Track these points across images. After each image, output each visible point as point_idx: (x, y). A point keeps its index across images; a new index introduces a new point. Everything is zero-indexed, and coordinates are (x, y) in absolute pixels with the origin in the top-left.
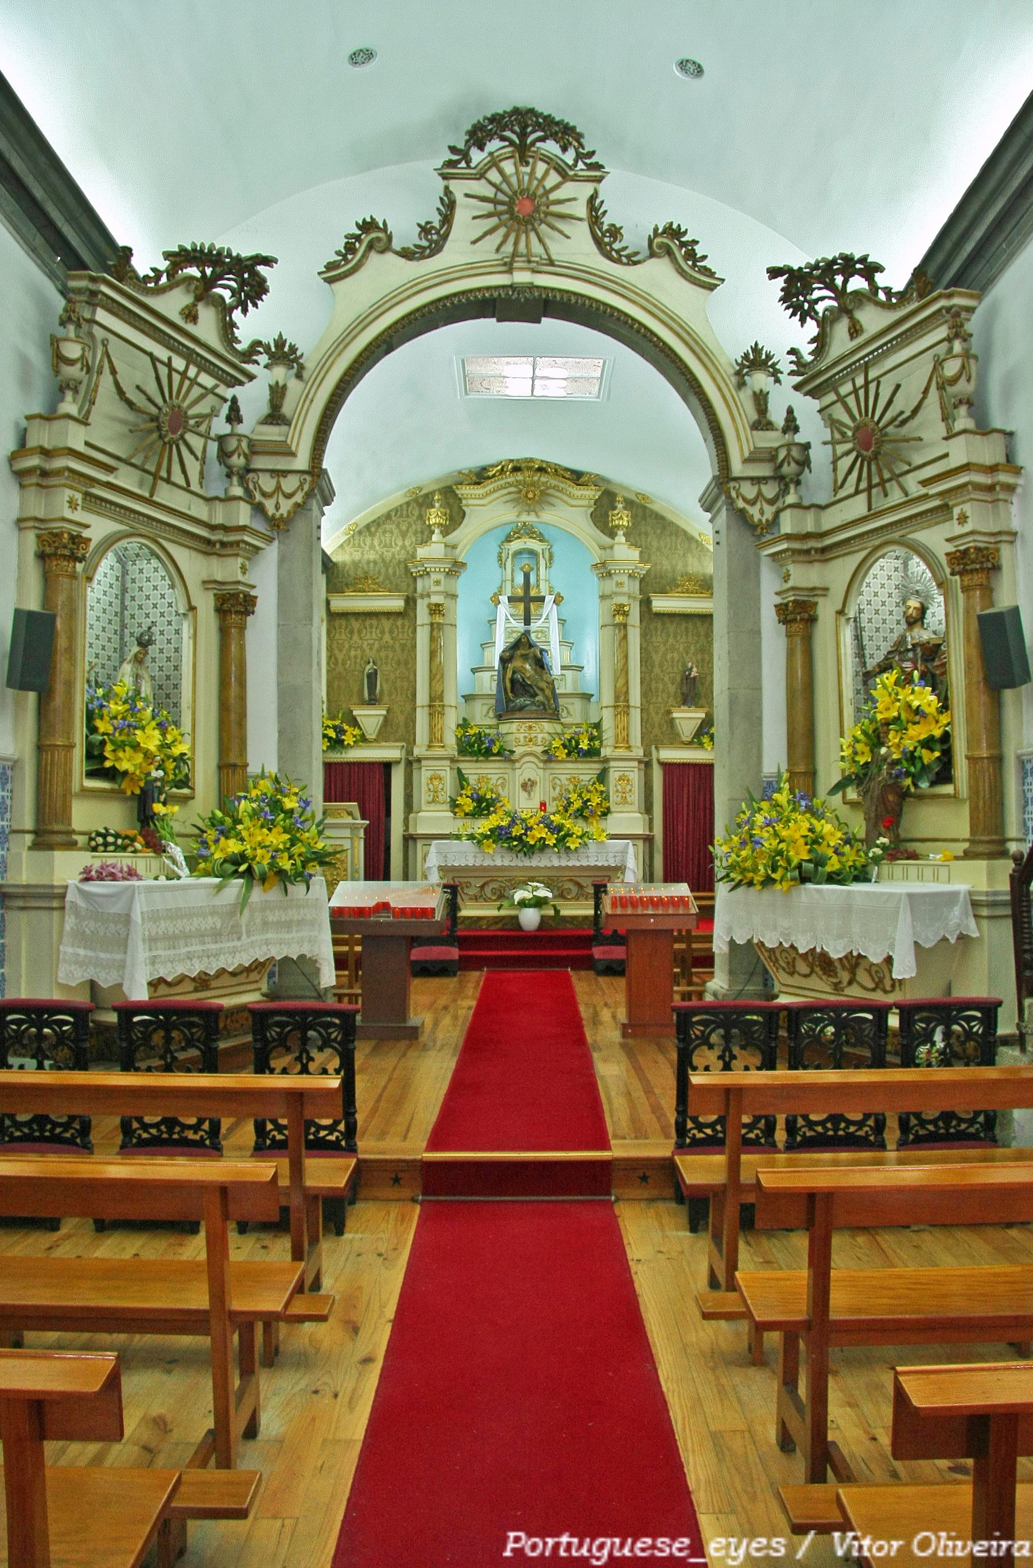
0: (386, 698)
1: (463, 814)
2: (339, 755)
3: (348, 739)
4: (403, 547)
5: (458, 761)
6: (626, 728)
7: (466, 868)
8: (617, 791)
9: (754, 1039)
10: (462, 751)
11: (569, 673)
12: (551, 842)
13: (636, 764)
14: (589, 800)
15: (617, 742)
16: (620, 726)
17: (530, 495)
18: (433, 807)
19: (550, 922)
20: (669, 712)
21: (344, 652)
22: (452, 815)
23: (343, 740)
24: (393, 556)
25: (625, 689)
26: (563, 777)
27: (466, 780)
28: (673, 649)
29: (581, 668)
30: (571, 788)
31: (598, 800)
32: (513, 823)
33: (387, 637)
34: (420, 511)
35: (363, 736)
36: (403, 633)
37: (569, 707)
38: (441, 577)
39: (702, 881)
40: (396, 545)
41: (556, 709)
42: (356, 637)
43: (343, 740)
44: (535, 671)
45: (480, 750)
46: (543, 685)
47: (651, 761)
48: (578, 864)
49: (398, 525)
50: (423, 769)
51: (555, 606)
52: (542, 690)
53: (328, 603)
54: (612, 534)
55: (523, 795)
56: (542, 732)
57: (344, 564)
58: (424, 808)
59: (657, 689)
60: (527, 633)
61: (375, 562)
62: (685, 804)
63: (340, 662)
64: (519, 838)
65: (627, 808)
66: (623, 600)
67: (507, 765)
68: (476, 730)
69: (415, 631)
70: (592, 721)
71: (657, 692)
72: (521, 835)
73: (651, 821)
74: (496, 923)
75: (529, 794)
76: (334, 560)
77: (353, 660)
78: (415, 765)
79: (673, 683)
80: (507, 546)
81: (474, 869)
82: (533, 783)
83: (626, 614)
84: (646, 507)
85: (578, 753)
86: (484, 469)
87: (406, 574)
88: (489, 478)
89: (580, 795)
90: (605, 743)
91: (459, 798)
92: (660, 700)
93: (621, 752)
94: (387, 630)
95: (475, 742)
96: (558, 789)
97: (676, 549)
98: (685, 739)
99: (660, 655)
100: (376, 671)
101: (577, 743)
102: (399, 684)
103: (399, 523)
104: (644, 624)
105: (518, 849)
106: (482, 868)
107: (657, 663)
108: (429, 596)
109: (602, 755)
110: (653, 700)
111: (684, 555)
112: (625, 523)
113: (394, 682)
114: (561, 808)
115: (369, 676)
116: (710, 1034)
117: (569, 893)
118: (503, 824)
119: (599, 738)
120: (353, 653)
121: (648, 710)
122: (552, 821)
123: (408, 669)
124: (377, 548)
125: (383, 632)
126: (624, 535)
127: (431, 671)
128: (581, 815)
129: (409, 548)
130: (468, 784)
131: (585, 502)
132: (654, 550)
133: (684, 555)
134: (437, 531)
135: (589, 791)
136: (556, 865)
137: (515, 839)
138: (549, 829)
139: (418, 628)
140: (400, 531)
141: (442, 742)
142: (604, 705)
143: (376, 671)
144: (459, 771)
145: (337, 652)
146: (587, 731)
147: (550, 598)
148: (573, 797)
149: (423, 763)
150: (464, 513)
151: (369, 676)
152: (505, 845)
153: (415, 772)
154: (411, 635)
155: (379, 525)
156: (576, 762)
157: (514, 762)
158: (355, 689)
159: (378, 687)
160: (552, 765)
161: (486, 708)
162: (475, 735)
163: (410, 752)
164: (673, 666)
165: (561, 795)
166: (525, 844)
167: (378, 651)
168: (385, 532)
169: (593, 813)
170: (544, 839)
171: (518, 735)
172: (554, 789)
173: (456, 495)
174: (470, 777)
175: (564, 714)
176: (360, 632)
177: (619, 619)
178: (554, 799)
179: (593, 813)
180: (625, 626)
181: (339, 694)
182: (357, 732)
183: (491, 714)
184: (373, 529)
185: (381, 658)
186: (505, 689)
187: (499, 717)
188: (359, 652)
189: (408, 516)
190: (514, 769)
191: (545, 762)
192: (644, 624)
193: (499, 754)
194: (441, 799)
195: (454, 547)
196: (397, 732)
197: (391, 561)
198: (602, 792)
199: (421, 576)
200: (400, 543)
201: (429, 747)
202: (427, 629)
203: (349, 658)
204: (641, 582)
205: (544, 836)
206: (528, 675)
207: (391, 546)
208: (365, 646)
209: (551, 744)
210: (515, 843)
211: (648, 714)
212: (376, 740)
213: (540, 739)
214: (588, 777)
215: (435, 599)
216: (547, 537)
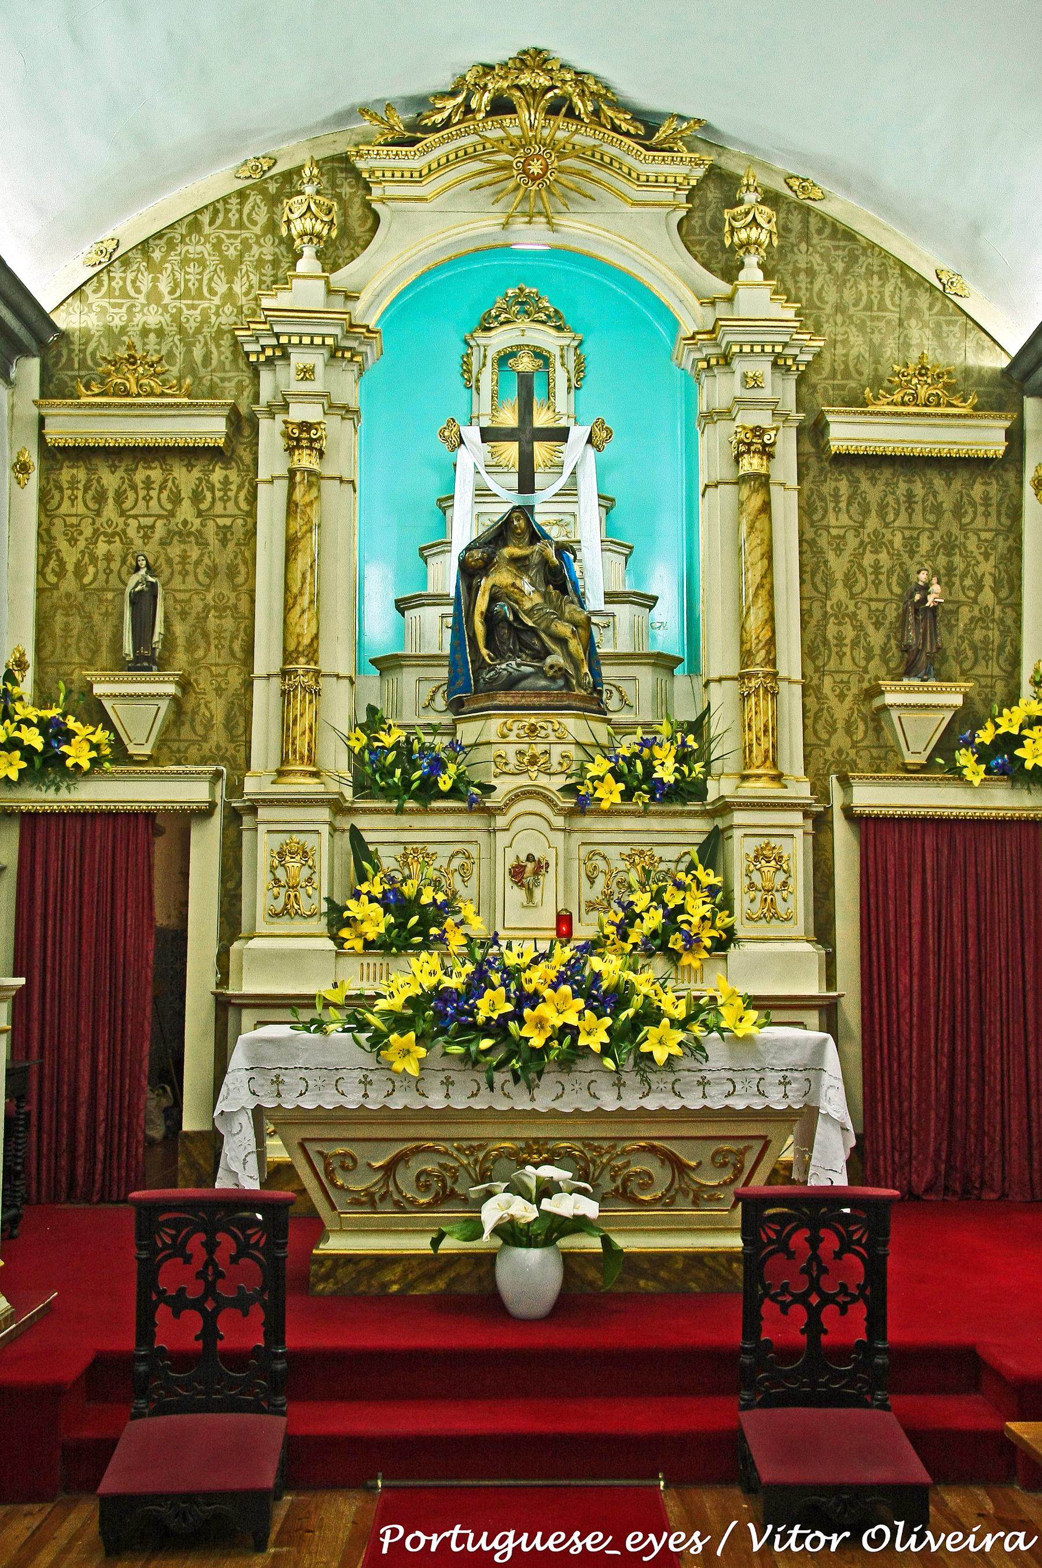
0: (181, 658)
1: (359, 945)
2: (51, 794)
3: (78, 754)
4: (229, 296)
5: (352, 811)
6: (771, 729)
7: (339, 1116)
8: (752, 885)
9: (853, 1242)
10: (361, 787)
11: (624, 612)
12: (595, 1038)
13: (797, 817)
14: (680, 909)
15: (746, 766)
16: (758, 724)
17: (535, 168)
18: (283, 926)
19: (592, 1274)
20: (876, 692)
21: (82, 544)
22: (330, 945)
23: (65, 756)
24: (205, 320)
25: (766, 635)
26: (612, 852)
27: (370, 857)
28: (877, 542)
29: (650, 602)
30: (633, 877)
31: (705, 910)
32: (478, 983)
33: (186, 511)
34: (271, 212)
35: (118, 744)
36: (225, 500)
37: (624, 686)
38: (317, 359)
39: (958, 1110)
40: (212, 292)
41: (596, 687)
42: (110, 510)
43: (65, 756)
44: (545, 595)
45: (407, 782)
46: (564, 629)
47: (829, 810)
48: (674, 1104)
49: (217, 246)
50: (262, 828)
51: (591, 451)
52: (562, 641)
53: (42, 421)
54: (730, 273)
55: (516, 895)
56: (561, 741)
57: (87, 336)
58: (261, 928)
59: (840, 638)
60: (526, 511)
61: (160, 333)
62: (916, 918)
63: (70, 567)
64: (497, 1028)
65: (775, 929)
66: (763, 418)
67: (476, 821)
68: (398, 735)
69: (253, 498)
70: (681, 719)
71: (840, 644)
72: (505, 1017)
73: (830, 962)
74: (431, 1277)
75: (530, 893)
76: (62, 321)
77: (102, 565)
78: (247, 821)
79: (877, 625)
80: (482, 339)
81: (362, 1116)
82: (541, 867)
83: (767, 452)
84: (808, 210)
85: (652, 792)
86: (421, 103)
87: (235, 361)
88: (435, 129)
89: (658, 897)
90: (716, 767)
91: (351, 903)
92: (847, 664)
93: (760, 788)
94: (186, 493)
95: (395, 764)
96: (601, 881)
97: (882, 307)
98: (910, 758)
99: (846, 556)
100: (153, 586)
101: (649, 769)
102: (212, 623)
103: (220, 241)
104: (807, 485)
105: (493, 1060)
106: (388, 1116)
107: (839, 576)
108: (286, 407)
109: (711, 797)
110: (832, 665)
111: (901, 324)
112: (764, 237)
113: (202, 619)
114: (610, 930)
115: (136, 599)
116: (789, 1235)
117: (644, 1187)
118: (454, 983)
119: (703, 754)
120: (102, 548)
121: (818, 688)
122: (597, 976)
123: (235, 588)
124: (167, 299)
125: (176, 499)
126: (761, 266)
127: (287, 588)
128: (664, 948)
129: (243, 301)
130: (377, 868)
131: (665, 195)
132: (828, 309)
133: (901, 324)
134: (309, 251)
135: (679, 886)
136: (610, 1108)
137: (487, 1029)
138: (589, 998)
139: (261, 487)
140: (224, 259)
141: (311, 761)
142: (714, 675)
143: (153, 586)
144: (355, 834)
145: (62, 544)
146: (672, 739)
147: (578, 434)
148: (641, 900)
149: (263, 813)
150: (377, 219)
151: (136, 599)
152: (457, 1050)
153: (246, 836)
154: (244, 506)
155: (171, 245)
156: (645, 813)
157: (491, 813)
158: (106, 635)
159: (159, 628)
160: (587, 822)
161: (427, 688)
162: (396, 746)
163: (235, 789)
164: (877, 584)
165: (608, 896)
166: (517, 1047)
167: (164, 543)
168: (185, 262)
169: (692, 942)
170: (575, 1031)
171: (502, 750)
172: (592, 881)
173: (357, 173)
174: (383, 851)
175: (613, 703)
176: (120, 497)
177: (752, 464)
178: (592, 906)
179: (692, 942)
180: (762, 482)
181: (66, 647)
182: (101, 736)
183: (440, 703)
184: (157, 255)
185: (169, 561)
186: (473, 639)
187: (456, 706)
188: (117, 547)
189: (241, 225)
190: (492, 832)
191: (569, 814)
192: (807, 485)
193: (454, 793)
194: (305, 906)
195: (350, 297)
196: (205, 739)
197: (198, 330)
198: (712, 890)
199: (270, 361)
200: (221, 288)
201: (281, 773)
202: (282, 486)
203: (94, 560)
204: (799, 382)
205: (572, 1019)
206: (528, 605)
207: (200, 295)
208: (132, 532)
209: (583, 769)
210: (486, 1043)
211: (820, 698)
212: (151, 759)
213: (555, 759)
214: (673, 853)
215: (299, 413)
216: (569, 321)
